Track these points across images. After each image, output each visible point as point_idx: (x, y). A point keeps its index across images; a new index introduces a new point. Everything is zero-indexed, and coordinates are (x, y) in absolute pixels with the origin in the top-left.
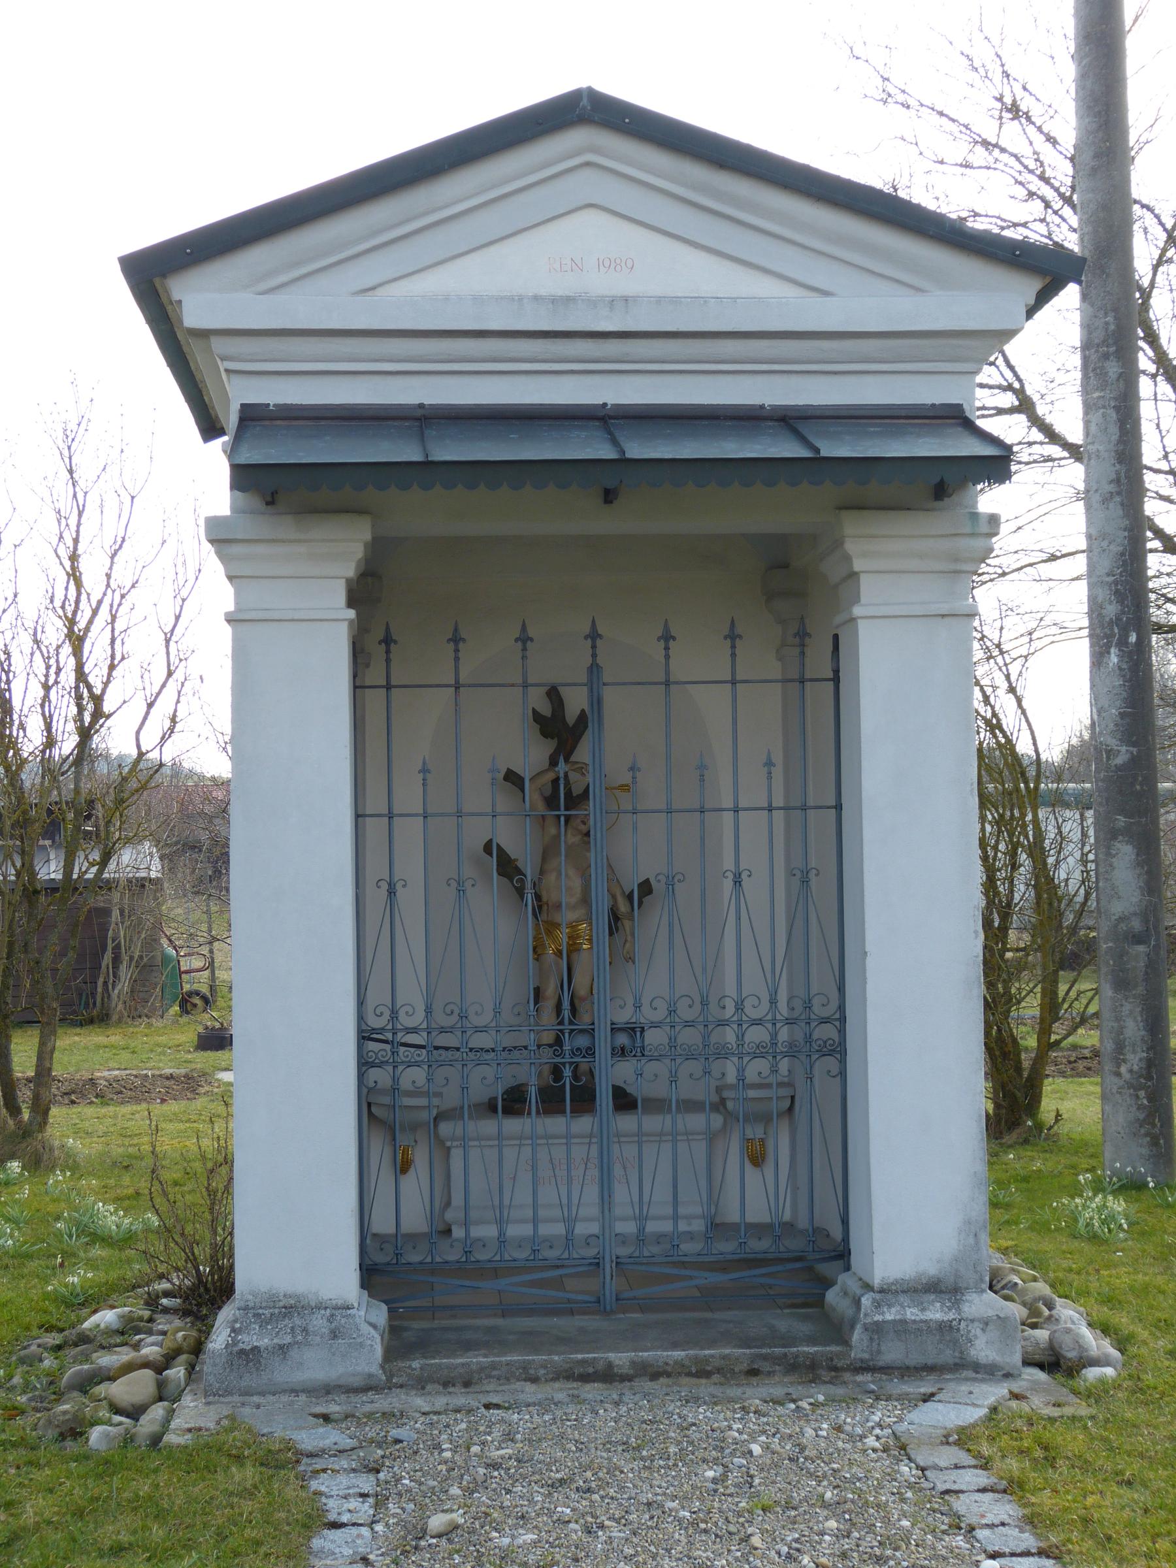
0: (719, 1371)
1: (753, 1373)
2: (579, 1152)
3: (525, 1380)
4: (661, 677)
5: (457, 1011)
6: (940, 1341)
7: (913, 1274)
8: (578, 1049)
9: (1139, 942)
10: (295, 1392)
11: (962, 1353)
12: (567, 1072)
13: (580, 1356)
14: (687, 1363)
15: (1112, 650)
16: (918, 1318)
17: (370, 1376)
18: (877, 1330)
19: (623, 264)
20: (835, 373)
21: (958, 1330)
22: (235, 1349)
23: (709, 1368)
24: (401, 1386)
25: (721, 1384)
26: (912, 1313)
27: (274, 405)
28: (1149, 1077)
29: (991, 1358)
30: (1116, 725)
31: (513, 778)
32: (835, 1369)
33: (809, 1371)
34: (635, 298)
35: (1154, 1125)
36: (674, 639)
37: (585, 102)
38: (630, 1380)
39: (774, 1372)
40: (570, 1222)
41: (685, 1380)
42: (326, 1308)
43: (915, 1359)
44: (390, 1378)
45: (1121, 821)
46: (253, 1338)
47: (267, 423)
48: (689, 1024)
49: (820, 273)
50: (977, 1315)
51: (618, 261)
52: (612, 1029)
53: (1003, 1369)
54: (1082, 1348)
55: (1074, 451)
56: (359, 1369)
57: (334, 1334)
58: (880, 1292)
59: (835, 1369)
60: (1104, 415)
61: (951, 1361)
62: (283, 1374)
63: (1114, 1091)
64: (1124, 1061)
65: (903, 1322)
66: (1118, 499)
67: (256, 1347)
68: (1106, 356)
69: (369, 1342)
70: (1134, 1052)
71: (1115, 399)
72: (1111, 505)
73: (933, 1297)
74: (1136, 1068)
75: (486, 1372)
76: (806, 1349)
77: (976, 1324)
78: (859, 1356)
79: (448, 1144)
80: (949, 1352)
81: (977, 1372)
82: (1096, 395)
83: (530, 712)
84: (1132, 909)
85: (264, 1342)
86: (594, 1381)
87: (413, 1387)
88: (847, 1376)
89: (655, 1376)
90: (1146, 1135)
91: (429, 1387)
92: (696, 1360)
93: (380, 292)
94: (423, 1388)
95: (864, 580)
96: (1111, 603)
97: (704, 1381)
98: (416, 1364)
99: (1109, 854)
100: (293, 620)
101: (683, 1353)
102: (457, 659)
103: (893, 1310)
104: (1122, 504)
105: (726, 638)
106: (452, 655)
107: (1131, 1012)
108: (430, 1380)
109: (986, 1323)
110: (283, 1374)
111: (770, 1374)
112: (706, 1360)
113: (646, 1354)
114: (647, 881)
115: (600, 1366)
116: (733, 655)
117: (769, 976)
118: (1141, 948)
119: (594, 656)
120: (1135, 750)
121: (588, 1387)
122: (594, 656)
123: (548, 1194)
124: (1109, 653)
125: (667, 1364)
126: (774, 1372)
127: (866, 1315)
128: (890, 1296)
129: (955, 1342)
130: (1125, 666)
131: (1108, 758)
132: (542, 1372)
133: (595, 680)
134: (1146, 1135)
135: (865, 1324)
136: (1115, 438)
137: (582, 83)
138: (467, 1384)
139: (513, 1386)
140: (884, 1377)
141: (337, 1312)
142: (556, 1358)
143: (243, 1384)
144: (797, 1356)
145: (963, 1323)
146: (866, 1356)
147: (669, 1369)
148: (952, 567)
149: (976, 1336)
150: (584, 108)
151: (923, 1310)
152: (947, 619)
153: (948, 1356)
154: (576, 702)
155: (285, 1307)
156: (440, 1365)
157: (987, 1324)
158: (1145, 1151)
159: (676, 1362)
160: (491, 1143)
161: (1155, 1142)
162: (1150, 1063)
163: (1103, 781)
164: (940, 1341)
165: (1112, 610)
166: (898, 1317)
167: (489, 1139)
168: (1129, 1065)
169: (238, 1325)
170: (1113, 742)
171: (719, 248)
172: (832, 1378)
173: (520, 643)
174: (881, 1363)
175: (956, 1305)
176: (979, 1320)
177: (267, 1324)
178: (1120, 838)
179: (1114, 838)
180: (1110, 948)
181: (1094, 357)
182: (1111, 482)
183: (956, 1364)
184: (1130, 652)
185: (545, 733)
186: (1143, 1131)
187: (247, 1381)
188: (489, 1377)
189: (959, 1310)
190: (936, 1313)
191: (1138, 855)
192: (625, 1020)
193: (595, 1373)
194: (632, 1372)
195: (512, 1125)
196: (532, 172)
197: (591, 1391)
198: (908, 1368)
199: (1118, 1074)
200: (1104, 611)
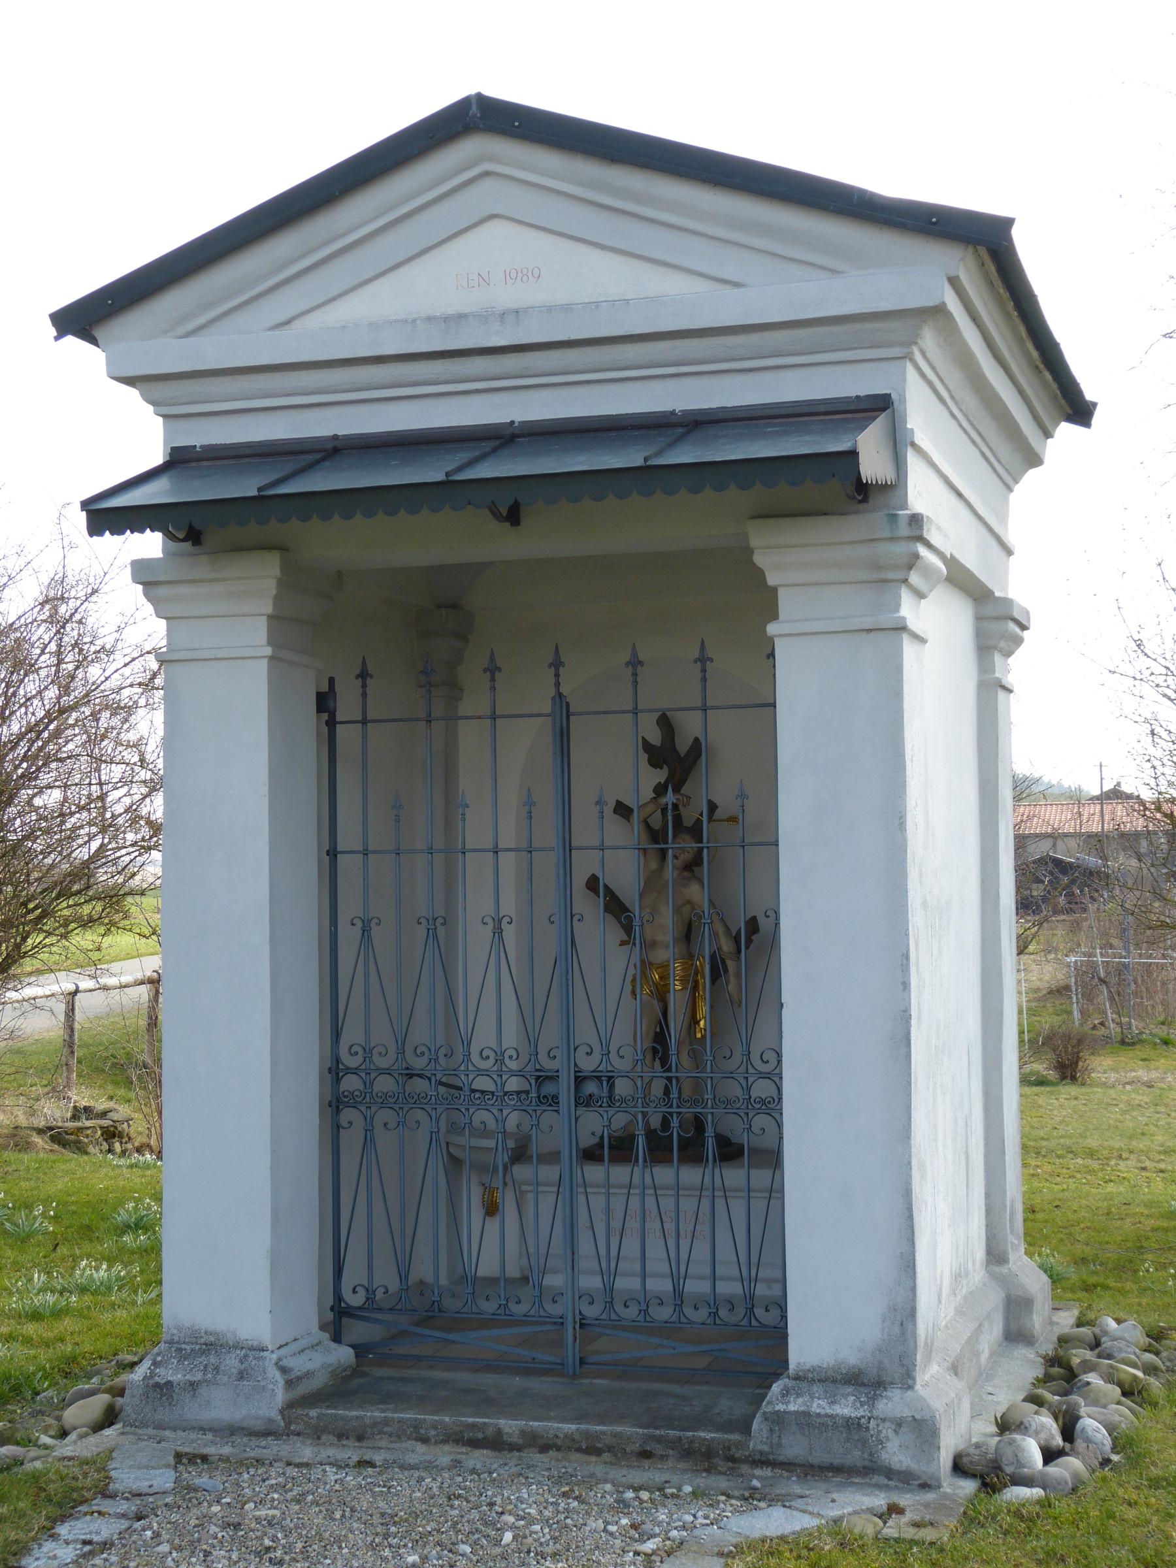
0: (610, 1449)
1: (645, 1455)
2: (688, 1205)
3: (416, 1440)
4: (630, 707)
6: (847, 1440)
8: (545, 1097)
10: (203, 1429)
11: (871, 1454)
12: (675, 1123)
13: (470, 1420)
14: (577, 1437)
16: (823, 1412)
17: (270, 1420)
18: (778, 1420)
19: (530, 274)
20: (750, 370)
21: (867, 1429)
22: (151, 1382)
23: (599, 1445)
24: (299, 1434)
25: (612, 1464)
26: (819, 1406)
27: (201, 447)
29: (905, 1464)
31: (622, 810)
32: (733, 1459)
33: (704, 1459)
34: (526, 310)
37: (474, 109)
38: (519, 1450)
39: (667, 1456)
40: (609, 1275)
41: (575, 1456)
42: (242, 1348)
43: (819, 1457)
44: (288, 1424)
46: (172, 1374)
47: (194, 464)
49: (731, 264)
50: (890, 1415)
51: (525, 272)
52: (576, 1078)
53: (919, 1478)
54: (1020, 1464)
56: (261, 1412)
57: (241, 1376)
58: (795, 1379)
59: (733, 1459)
61: (860, 1464)
62: (193, 1410)
65: (807, 1414)
67: (170, 1382)
69: (271, 1386)
73: (851, 1389)
75: (380, 1427)
76: (702, 1434)
77: (888, 1424)
78: (759, 1447)
79: (524, 1188)
80: (857, 1453)
81: (890, 1479)
83: (640, 740)
85: (177, 1378)
86: (483, 1448)
87: (309, 1436)
88: (745, 1469)
89: (544, 1448)
91: (324, 1438)
92: (587, 1435)
93: (296, 324)
94: (319, 1438)
95: (782, 594)
97: (594, 1458)
98: (313, 1413)
100: (216, 659)
101: (574, 1427)
102: (635, 683)
103: (800, 1400)
105: (550, 666)
106: (553, 680)
108: (325, 1430)
109: (899, 1424)
110: (193, 1410)
111: (663, 1458)
112: (597, 1436)
113: (536, 1424)
114: (754, 919)
115: (490, 1432)
116: (364, 695)
121: (478, 1453)
123: (655, 1249)
125: (556, 1436)
126: (667, 1456)
127: (769, 1403)
128: (804, 1385)
129: (864, 1442)
132: (433, 1432)
135: (765, 1413)
137: (471, 91)
138: (360, 1438)
139: (404, 1445)
140: (786, 1474)
141: (250, 1353)
142: (447, 1419)
143: (157, 1417)
144: (692, 1441)
145: (873, 1423)
146: (766, 1448)
147: (559, 1442)
148: (876, 576)
149: (888, 1439)
150: (474, 116)
151: (834, 1403)
152: (873, 634)
153: (855, 1457)
154: (689, 726)
155: (206, 1344)
156: (335, 1416)
157: (900, 1425)
159: (566, 1436)
160: (549, 1189)
164: (847, 1440)
166: (802, 1409)
167: (598, 1187)
169: (159, 1359)
171: (623, 247)
172: (729, 1469)
173: (699, 663)
174: (781, 1458)
175: (872, 1400)
176: (892, 1420)
177: (185, 1359)
183: (865, 1467)
185: (654, 763)
187: (162, 1415)
188: (381, 1432)
189: (872, 1407)
190: (845, 1408)
192: (592, 1069)
193: (484, 1439)
194: (521, 1441)
195: (620, 1173)
196: (430, 189)
197: (477, 1458)
198: (812, 1466)
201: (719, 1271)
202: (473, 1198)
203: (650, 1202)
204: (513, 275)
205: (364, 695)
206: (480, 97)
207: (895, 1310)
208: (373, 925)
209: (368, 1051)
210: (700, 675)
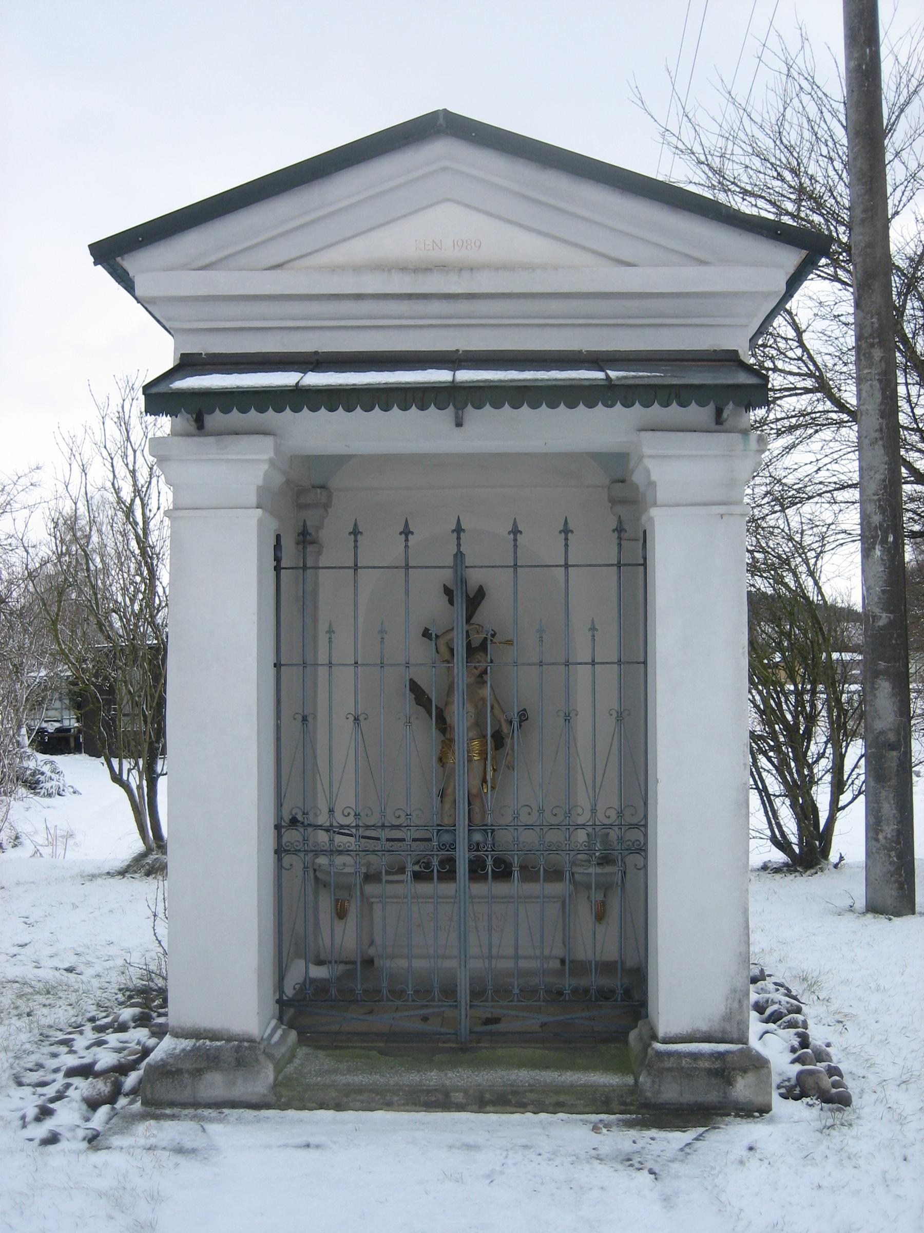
5: (352, 814)
7: (689, 1031)
9: (893, 749)
15: (877, 547)
23: (524, 1100)
28: (898, 843)
30: (879, 599)
35: (901, 876)
36: (521, 532)
45: (882, 665)
47: (199, 367)
48: (528, 827)
51: (469, 242)
52: (469, 830)
55: (854, 415)
60: (871, 386)
63: (874, 851)
64: (881, 831)
66: (881, 442)
68: (872, 345)
70: (888, 825)
71: (879, 374)
72: (876, 447)
74: (889, 836)
79: (372, 900)
82: (865, 372)
84: (888, 726)
90: (895, 882)
95: (253, 500)
96: (876, 514)
99: (873, 688)
104: (884, 446)
107: (887, 798)
117: (590, 789)
118: (894, 753)
119: (459, 545)
120: (892, 616)
122: (459, 545)
124: (874, 548)
130: (885, 558)
131: (873, 621)
133: (459, 563)
134: (895, 882)
136: (879, 401)
137: (441, 107)
158: (894, 893)
161: (901, 888)
162: (899, 833)
163: (869, 637)
165: (877, 519)
168: (884, 834)
170: (877, 611)
173: (403, 536)
178: (881, 677)
179: (877, 677)
180: (873, 753)
181: (864, 346)
182: (876, 431)
184: (889, 548)
186: (893, 879)
191: (893, 689)
199: (877, 840)
200: (871, 520)
202: (326, 905)
204: (460, 243)
206: (445, 110)
207: (735, 992)
210: (563, 542)
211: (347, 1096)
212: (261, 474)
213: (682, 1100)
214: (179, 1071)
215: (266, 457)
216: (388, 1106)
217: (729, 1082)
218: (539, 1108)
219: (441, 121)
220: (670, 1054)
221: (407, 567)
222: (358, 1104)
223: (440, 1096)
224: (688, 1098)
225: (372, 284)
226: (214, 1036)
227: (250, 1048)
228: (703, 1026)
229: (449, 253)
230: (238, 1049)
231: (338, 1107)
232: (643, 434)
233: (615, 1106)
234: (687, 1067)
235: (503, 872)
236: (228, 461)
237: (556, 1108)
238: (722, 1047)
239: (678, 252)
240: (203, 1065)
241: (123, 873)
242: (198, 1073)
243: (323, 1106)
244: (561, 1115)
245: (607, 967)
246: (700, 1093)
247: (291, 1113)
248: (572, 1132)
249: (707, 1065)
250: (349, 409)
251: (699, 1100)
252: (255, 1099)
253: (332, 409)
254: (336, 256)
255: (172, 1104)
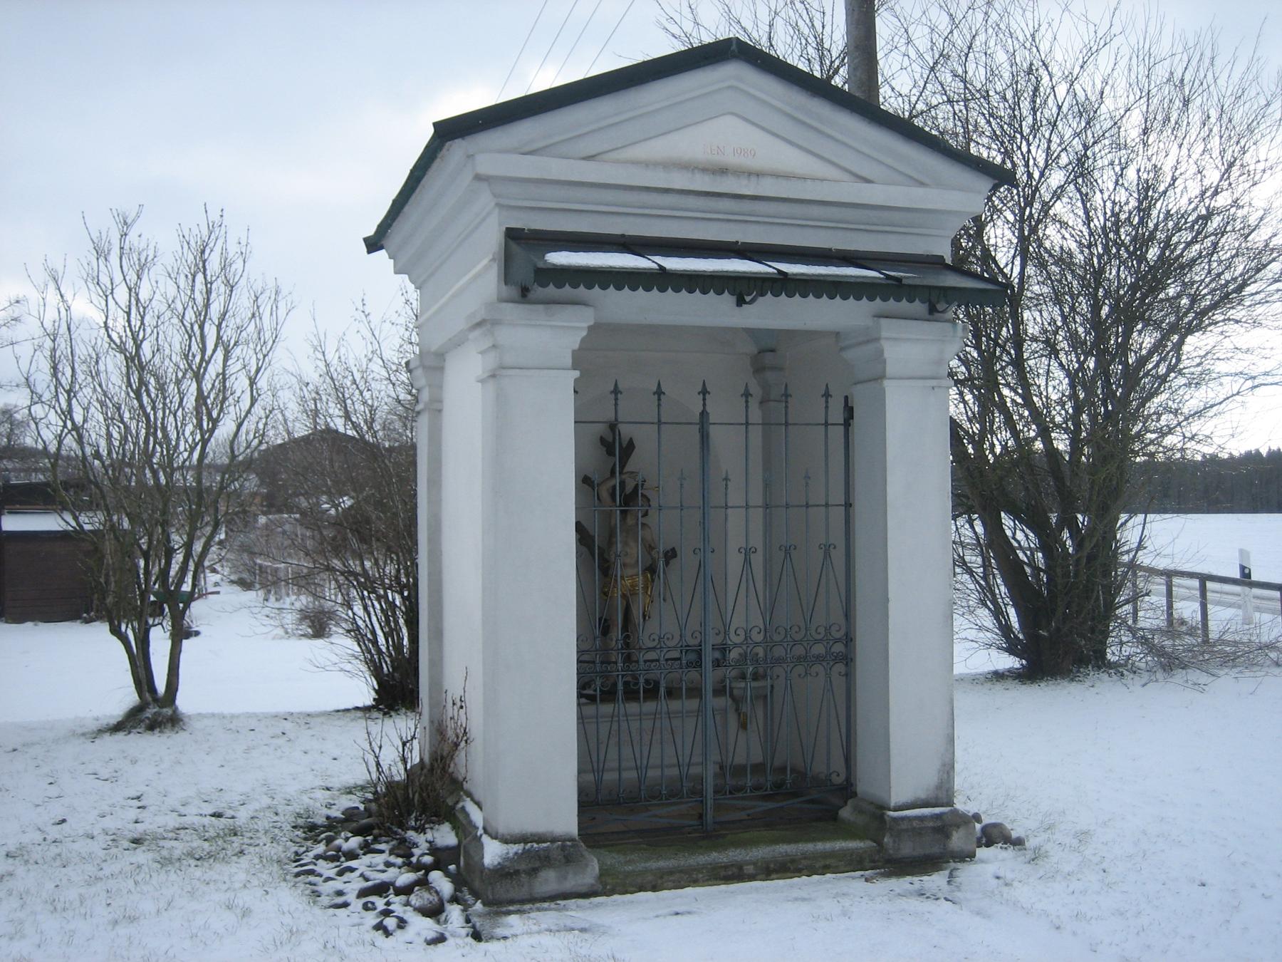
4: (663, 427)
95: (568, 361)
116: (747, 407)
119: (704, 405)
122: (704, 405)
123: (627, 751)
201: (624, 764)
203: (624, 725)
205: (747, 407)
208: (792, 551)
209: (828, 630)
211: (661, 878)
212: (579, 340)
213: (915, 854)
214: (517, 872)
215: (585, 325)
216: (695, 882)
217: (948, 836)
218: (811, 871)
219: (734, 47)
220: (903, 819)
221: (659, 423)
222: (670, 884)
223: (735, 870)
224: (919, 852)
225: (680, 181)
226: (539, 838)
227: (572, 846)
228: (922, 795)
229: (730, 159)
230: (563, 848)
231: (655, 888)
232: (883, 321)
233: (867, 864)
234: (916, 829)
235: (652, 692)
236: (552, 327)
237: (823, 870)
238: (937, 810)
239: (901, 173)
240: (537, 864)
241: (118, 728)
242: (534, 872)
243: (642, 888)
244: (829, 875)
245: (758, 768)
246: (925, 844)
247: (616, 897)
248: (853, 885)
249: (931, 824)
250: (704, 292)
251: (927, 852)
252: (584, 890)
253: (691, 291)
254: (640, 152)
255: (512, 902)
